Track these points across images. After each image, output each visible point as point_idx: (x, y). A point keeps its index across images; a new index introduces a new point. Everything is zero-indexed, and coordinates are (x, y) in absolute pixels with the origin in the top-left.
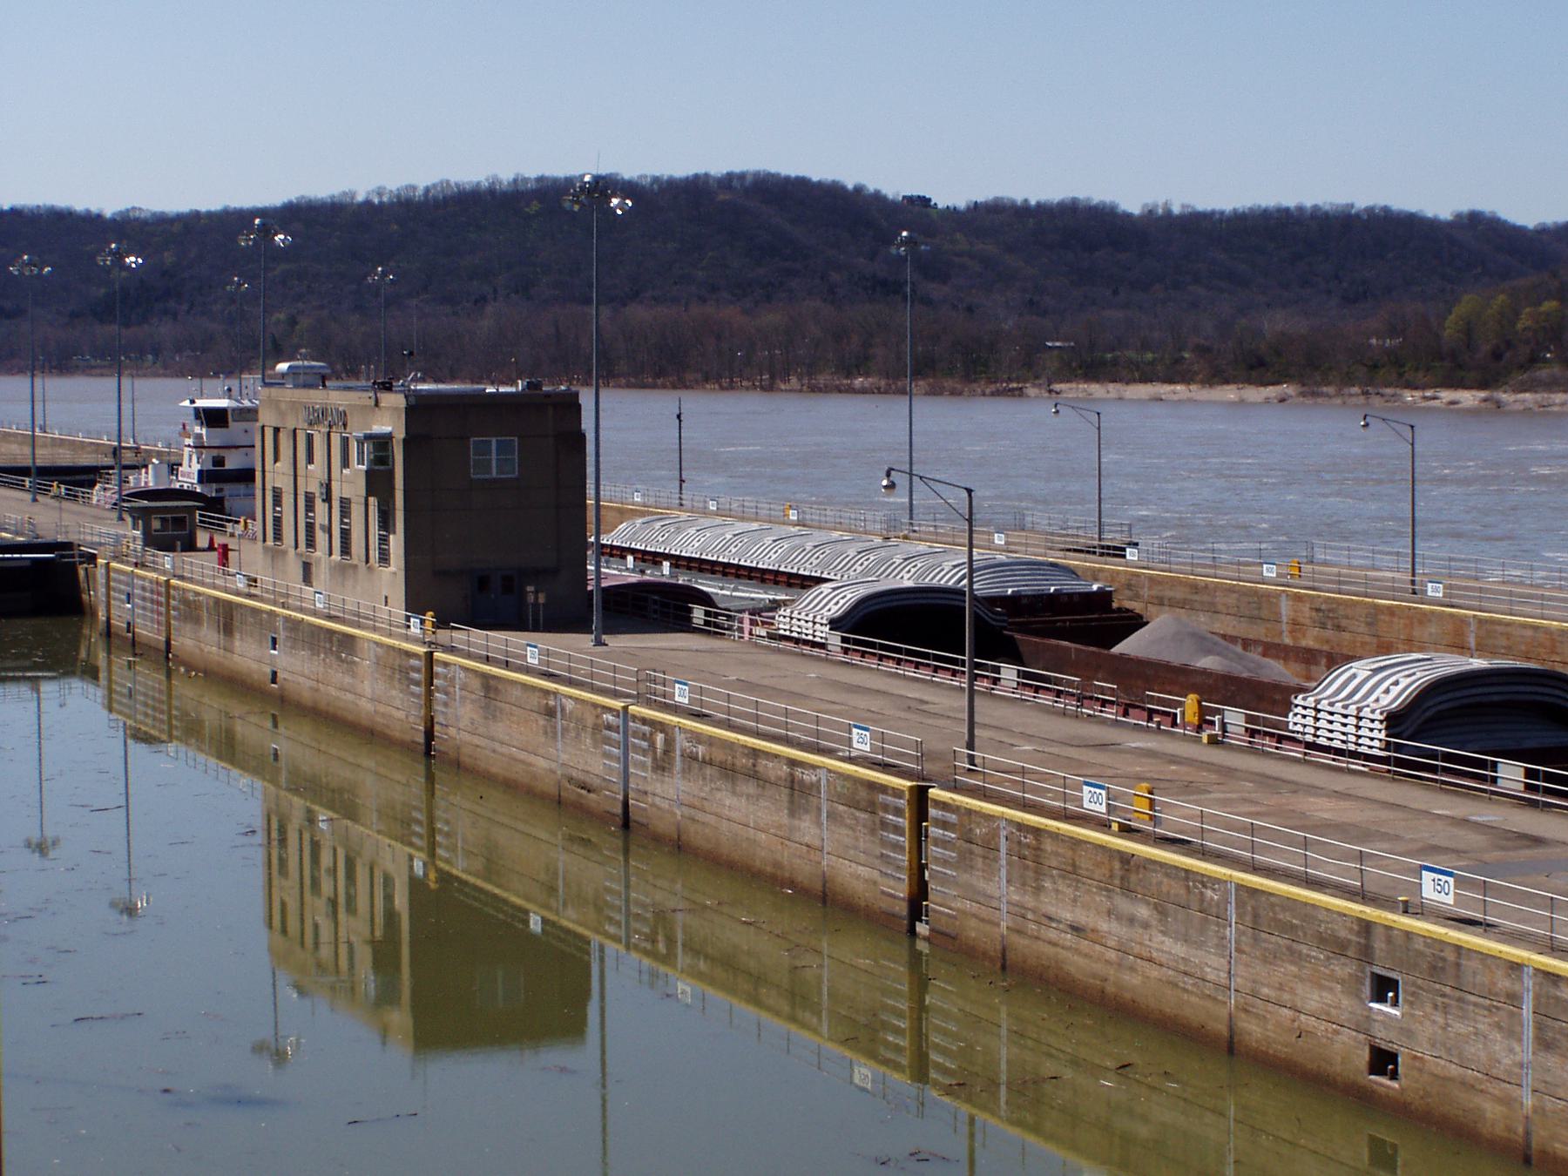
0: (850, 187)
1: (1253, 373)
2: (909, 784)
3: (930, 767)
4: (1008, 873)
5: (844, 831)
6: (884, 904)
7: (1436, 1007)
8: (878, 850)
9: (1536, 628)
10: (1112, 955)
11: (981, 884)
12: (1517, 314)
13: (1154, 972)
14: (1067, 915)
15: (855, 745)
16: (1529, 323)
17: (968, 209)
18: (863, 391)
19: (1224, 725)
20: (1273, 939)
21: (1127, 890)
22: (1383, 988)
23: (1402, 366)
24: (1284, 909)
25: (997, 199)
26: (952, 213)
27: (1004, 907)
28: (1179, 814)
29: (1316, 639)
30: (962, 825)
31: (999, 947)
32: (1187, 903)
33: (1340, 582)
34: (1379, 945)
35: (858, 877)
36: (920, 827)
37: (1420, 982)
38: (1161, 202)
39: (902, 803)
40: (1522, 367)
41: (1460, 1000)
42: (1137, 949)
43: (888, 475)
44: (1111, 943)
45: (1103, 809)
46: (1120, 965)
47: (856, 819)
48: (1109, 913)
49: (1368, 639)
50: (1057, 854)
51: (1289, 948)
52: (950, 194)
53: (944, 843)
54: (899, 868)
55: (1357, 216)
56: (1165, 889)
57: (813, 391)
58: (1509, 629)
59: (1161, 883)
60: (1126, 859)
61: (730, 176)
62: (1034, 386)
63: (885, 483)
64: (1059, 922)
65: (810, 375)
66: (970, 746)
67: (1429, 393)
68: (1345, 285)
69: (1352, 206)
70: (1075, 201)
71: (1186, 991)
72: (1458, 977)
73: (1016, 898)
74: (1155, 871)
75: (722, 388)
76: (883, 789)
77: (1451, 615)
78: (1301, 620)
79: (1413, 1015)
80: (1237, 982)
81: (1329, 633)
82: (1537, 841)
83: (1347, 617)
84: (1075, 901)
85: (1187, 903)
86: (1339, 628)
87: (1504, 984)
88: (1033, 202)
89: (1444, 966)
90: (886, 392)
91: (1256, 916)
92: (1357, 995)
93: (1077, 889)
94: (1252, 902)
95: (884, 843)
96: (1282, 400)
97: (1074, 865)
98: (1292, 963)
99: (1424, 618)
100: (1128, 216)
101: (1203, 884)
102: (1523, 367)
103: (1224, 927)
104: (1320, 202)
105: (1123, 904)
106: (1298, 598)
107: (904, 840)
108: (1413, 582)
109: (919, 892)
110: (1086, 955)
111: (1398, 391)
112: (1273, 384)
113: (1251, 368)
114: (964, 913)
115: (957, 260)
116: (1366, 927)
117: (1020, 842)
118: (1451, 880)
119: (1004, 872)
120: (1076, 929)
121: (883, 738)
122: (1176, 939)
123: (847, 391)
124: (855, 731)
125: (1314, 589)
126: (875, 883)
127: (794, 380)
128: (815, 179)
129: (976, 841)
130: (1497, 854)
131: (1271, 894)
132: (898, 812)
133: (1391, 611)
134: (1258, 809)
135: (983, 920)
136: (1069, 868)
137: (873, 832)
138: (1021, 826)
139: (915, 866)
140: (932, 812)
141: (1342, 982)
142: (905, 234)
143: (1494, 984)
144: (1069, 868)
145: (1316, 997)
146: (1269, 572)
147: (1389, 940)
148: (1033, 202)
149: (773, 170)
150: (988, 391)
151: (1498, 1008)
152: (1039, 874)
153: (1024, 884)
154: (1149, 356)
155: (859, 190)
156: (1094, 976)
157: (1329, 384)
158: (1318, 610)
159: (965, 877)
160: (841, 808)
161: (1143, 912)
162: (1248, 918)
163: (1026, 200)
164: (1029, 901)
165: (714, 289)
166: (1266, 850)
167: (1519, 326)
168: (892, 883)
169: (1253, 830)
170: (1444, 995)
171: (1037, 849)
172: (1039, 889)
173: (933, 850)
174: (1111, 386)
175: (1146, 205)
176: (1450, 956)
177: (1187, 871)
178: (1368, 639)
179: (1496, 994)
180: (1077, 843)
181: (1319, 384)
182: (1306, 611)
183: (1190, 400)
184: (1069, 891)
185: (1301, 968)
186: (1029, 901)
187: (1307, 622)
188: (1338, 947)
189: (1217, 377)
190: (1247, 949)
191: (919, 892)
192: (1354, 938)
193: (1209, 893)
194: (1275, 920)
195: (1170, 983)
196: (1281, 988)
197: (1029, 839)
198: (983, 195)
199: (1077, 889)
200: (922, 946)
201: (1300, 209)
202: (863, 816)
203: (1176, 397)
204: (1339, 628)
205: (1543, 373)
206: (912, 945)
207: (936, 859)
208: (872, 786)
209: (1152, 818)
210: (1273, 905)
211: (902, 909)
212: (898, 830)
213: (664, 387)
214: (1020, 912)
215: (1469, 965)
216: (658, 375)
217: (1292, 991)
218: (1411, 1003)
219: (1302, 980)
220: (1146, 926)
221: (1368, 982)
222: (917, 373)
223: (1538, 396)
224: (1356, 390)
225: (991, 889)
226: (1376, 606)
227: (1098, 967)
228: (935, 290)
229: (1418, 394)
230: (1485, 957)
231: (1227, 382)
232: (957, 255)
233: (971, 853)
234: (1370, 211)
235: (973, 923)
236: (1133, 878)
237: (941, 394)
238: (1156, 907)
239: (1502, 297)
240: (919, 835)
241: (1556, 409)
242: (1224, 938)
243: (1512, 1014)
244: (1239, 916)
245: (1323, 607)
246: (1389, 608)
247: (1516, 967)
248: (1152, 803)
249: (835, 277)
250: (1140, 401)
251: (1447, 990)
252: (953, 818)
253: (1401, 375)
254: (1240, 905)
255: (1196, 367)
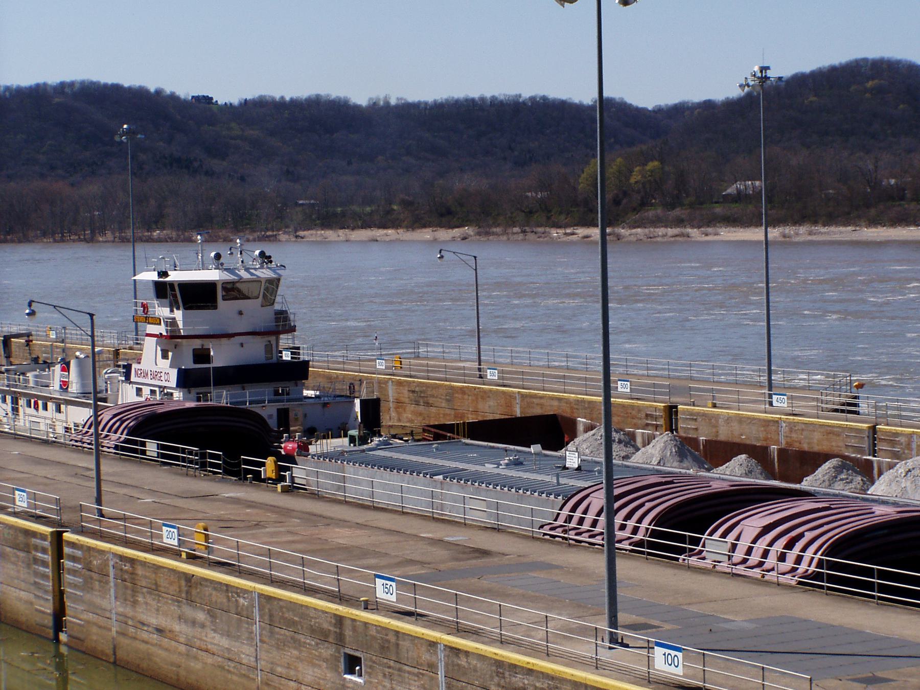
0: (152, 90)
1: (443, 219)
2: (51, 530)
3: (65, 518)
4: (116, 592)
5: (12, 566)
6: (38, 618)
7: (385, 675)
8: (32, 579)
9: (559, 399)
10: (183, 648)
11: (98, 601)
12: (631, 171)
13: (210, 660)
14: (153, 621)
15: (18, 503)
16: (639, 178)
17: (241, 104)
18: (159, 240)
19: (292, 478)
20: (283, 632)
21: (190, 601)
22: (352, 664)
23: (550, 211)
24: (288, 610)
25: (261, 97)
26: (228, 107)
27: (114, 617)
28: (226, 546)
29: (413, 412)
30: (85, 559)
31: (112, 646)
32: (227, 608)
33: (428, 371)
34: (348, 632)
35: (20, 599)
36: (59, 563)
37: (374, 658)
38: (382, 97)
39: (47, 544)
40: (634, 209)
41: (400, 670)
42: (198, 643)
43: (30, 305)
44: (182, 640)
45: (175, 543)
46: (187, 655)
47: (18, 557)
48: (180, 618)
49: (448, 411)
50: (146, 577)
51: (292, 638)
52: (228, 93)
53: (74, 572)
54: (46, 592)
55: (524, 103)
56: (214, 600)
57: (123, 241)
58: (542, 401)
59: (211, 595)
60: (189, 578)
61: (63, 84)
62: (285, 233)
63: (27, 311)
64: (148, 626)
65: (121, 230)
66: (99, 501)
67: (568, 231)
68: (516, 153)
69: (520, 96)
70: (318, 97)
71: (229, 671)
72: (397, 653)
73: (121, 610)
74: (206, 586)
75: (55, 241)
76: (34, 534)
77: (504, 392)
78: (403, 399)
79: (371, 682)
80: (261, 664)
81: (421, 408)
82: (485, 553)
83: (433, 396)
84: (158, 610)
85: (227, 608)
86: (428, 404)
87: (426, 657)
88: (288, 99)
89: (389, 644)
90: (177, 241)
91: (271, 616)
92: (335, 669)
93: (159, 601)
94: (268, 606)
95: (36, 574)
96: (464, 239)
97: (156, 584)
98: (295, 648)
99: (485, 395)
100: (357, 108)
101: (237, 593)
102: (635, 210)
103: (252, 625)
104: (496, 94)
105: (188, 611)
106: (400, 383)
107: (48, 571)
108: (480, 370)
109: (59, 613)
110: (166, 650)
111: (547, 229)
112: (458, 227)
113: (442, 215)
114: (88, 622)
115: (233, 142)
116: (340, 620)
117: (121, 570)
118: (394, 584)
119: (112, 591)
120: (160, 631)
121: (35, 497)
122: (222, 635)
123: (147, 241)
124: (17, 492)
125: (411, 377)
126: (31, 603)
127: (109, 236)
128: (126, 85)
129: (94, 570)
130: (452, 564)
131: (280, 600)
132: (44, 551)
133: (462, 390)
134: (296, 538)
135: (100, 627)
136: (154, 587)
137: (28, 566)
138: (122, 558)
139: (57, 594)
140: (67, 550)
141: (326, 660)
142: (125, 126)
143: (420, 657)
144: (154, 587)
145: (311, 673)
146: (381, 365)
147: (354, 629)
148: (288, 99)
149: (94, 79)
150: (251, 238)
151: (423, 674)
152: (134, 591)
153: (125, 600)
154: (368, 209)
155: (159, 92)
156: (172, 664)
157: (498, 225)
158: (413, 392)
159: (88, 596)
160: (8, 549)
161: (201, 616)
162: (267, 617)
163: (282, 97)
164: (129, 611)
165: (52, 168)
166: (281, 569)
167: (632, 181)
168: (42, 602)
169: (269, 554)
170: (389, 667)
171: (132, 574)
172: (135, 603)
173: (68, 578)
174: (341, 232)
175: (370, 99)
176: (392, 639)
177: (227, 585)
178: (448, 411)
179: (421, 665)
180: (157, 568)
181: (490, 226)
182: (405, 394)
183: (398, 240)
184: (154, 603)
185: (301, 651)
186: (129, 611)
187: (407, 400)
188: (322, 635)
189: (417, 223)
190: (266, 639)
191: (59, 613)
192: (332, 628)
193: (241, 601)
194: (283, 617)
195: (219, 666)
196: (288, 667)
197: (127, 567)
198: (251, 94)
199: (159, 601)
200: (63, 649)
201: (482, 99)
202: (22, 554)
203: (388, 239)
204: (428, 404)
205: (651, 213)
206: (57, 649)
207: (70, 584)
208: (28, 533)
209: (207, 547)
210: (281, 607)
211: (49, 621)
212: (44, 564)
213: (12, 241)
214: (124, 619)
215: (405, 644)
216: (8, 233)
217: (296, 669)
218: (370, 674)
219: (302, 661)
220: (203, 626)
221: (342, 660)
222: (199, 226)
223: (647, 230)
224: (516, 229)
225: (105, 604)
226: (452, 388)
227: (175, 658)
228: (217, 164)
229: (561, 231)
230: (414, 638)
231: (424, 226)
232: (232, 138)
233: (91, 578)
234: (532, 99)
235: (95, 629)
236: (194, 592)
237: (216, 241)
238: (209, 612)
239: (619, 160)
240: (58, 568)
241: (659, 239)
242: (252, 633)
243: (432, 679)
244: (261, 616)
245: (417, 389)
246: (462, 388)
247: (433, 644)
248: (207, 537)
249: (142, 157)
250: (361, 242)
251: (392, 663)
252: (79, 553)
253: (548, 218)
254: (261, 609)
255: (402, 216)
